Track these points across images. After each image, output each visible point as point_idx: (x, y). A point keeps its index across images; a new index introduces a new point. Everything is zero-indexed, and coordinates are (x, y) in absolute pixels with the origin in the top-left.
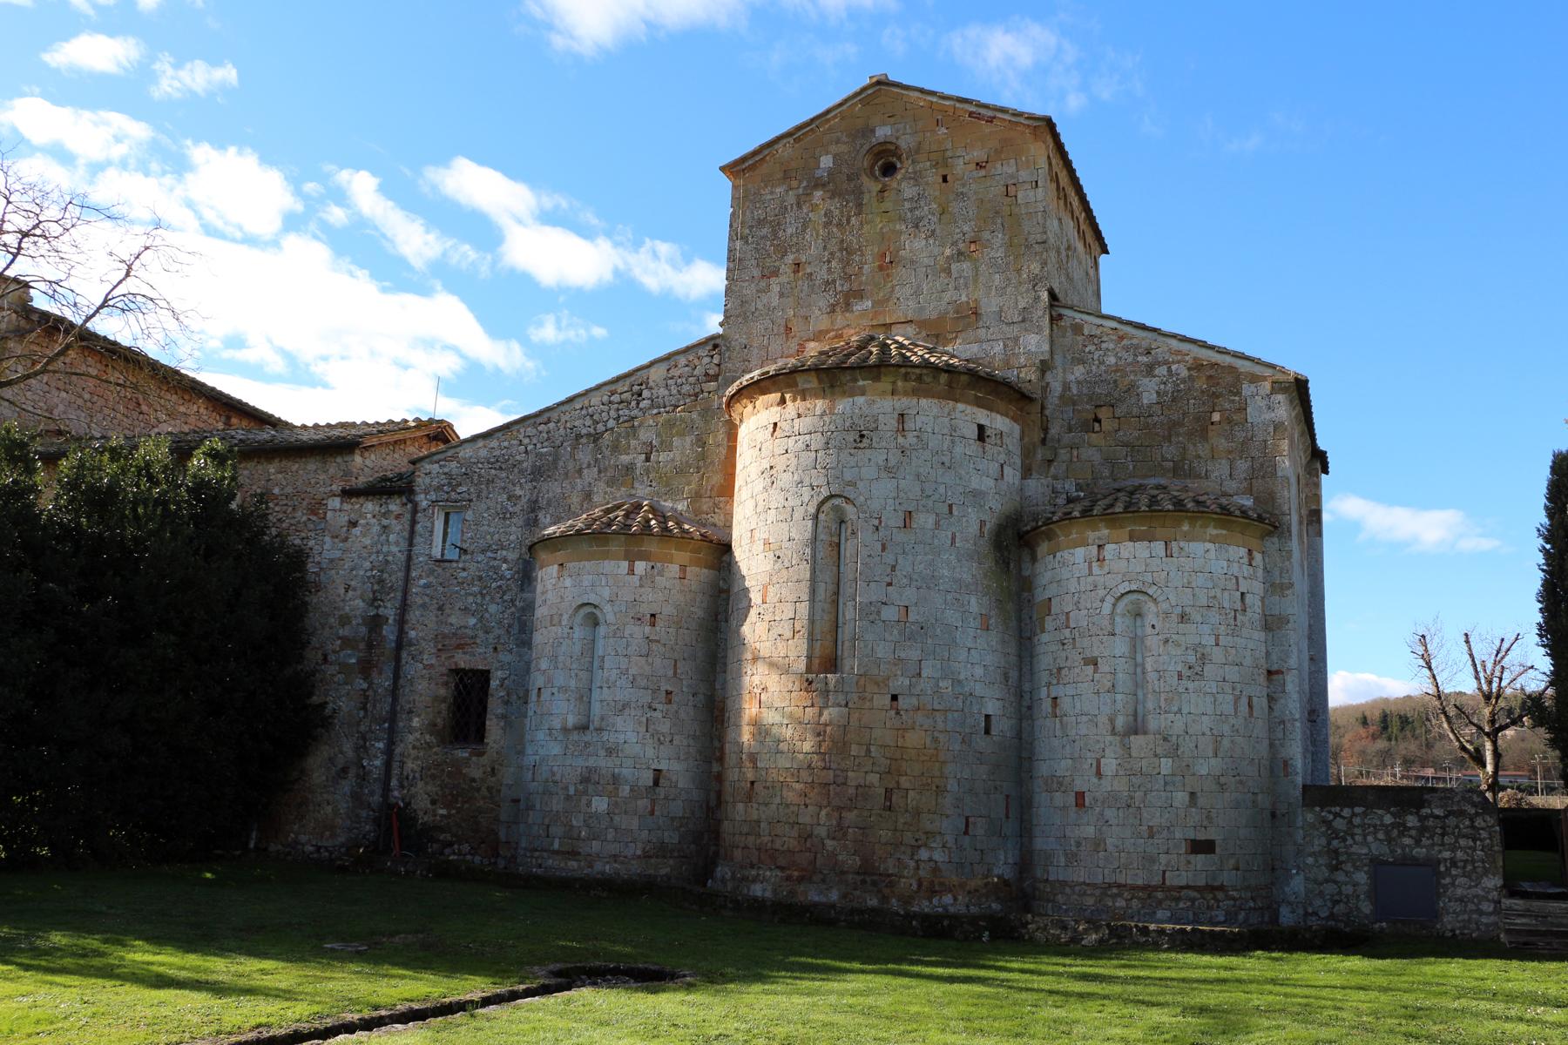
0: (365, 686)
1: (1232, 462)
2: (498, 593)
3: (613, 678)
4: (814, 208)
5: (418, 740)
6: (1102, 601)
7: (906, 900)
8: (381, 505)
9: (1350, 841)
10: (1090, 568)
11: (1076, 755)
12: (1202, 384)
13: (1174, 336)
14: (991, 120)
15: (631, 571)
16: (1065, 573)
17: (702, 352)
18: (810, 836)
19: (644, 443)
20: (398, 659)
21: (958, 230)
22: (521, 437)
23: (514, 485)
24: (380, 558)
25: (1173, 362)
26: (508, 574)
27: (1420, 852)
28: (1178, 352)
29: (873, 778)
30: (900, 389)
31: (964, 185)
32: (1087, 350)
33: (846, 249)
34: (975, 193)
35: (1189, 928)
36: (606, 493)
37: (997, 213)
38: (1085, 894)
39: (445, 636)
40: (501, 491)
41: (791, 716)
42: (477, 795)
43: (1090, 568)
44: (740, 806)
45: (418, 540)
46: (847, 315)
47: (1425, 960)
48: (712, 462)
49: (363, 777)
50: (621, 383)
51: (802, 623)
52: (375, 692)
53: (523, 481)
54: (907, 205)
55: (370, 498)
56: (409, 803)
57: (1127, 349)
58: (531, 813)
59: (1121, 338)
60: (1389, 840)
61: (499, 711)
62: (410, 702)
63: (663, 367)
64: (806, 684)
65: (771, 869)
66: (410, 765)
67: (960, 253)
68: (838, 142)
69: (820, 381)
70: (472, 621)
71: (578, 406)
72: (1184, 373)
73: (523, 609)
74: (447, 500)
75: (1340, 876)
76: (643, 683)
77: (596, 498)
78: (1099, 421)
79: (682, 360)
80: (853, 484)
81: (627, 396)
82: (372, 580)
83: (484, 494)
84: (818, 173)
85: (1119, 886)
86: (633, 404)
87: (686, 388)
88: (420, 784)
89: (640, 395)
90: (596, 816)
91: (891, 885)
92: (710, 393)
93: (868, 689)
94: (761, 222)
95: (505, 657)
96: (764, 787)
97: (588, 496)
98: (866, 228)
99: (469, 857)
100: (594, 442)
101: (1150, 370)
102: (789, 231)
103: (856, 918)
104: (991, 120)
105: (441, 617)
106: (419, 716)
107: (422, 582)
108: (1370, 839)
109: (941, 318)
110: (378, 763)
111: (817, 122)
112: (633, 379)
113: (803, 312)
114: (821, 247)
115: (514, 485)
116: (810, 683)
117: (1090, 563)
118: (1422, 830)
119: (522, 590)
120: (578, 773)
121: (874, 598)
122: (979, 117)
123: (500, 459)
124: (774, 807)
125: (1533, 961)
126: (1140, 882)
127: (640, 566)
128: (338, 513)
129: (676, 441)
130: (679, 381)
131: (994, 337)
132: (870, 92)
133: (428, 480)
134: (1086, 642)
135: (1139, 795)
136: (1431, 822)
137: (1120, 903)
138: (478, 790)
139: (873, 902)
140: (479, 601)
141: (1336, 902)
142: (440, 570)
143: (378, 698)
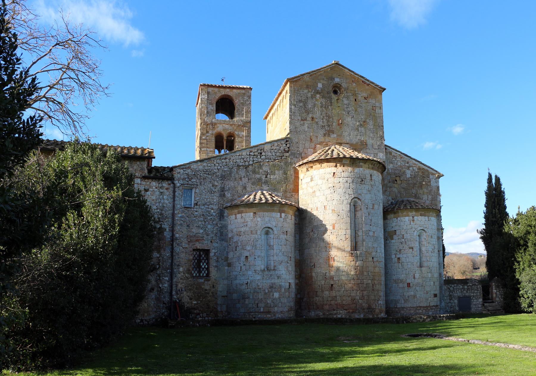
0: (158, 255)
1: (428, 196)
2: (211, 221)
3: (278, 253)
4: (317, 100)
5: (182, 276)
6: (414, 232)
7: (377, 315)
8: (159, 184)
9: (454, 293)
10: (410, 223)
11: (407, 273)
12: (420, 174)
13: (414, 159)
14: (368, 85)
15: (281, 217)
16: (402, 224)
17: (283, 142)
18: (355, 299)
19: (265, 171)
20: (172, 245)
21: (360, 117)
22: (215, 163)
23: (214, 181)
24: (161, 205)
25: (414, 167)
26: (214, 214)
27: (467, 294)
28: (415, 164)
29: (370, 281)
30: (370, 167)
31: (361, 104)
32: (393, 160)
33: (328, 116)
34: (364, 107)
35: (448, 315)
36: (251, 187)
37: (371, 114)
38: (411, 310)
39: (191, 237)
40: (209, 183)
41: (346, 264)
42: (208, 295)
43: (410, 223)
44: (327, 293)
45: (176, 199)
46: (329, 138)
47: (492, 317)
48: (290, 181)
49: (160, 291)
50: (254, 149)
51: (348, 236)
52: (163, 258)
53: (217, 180)
54: (345, 106)
55: (154, 180)
56: (181, 300)
57: (403, 161)
58: (247, 300)
59: (401, 158)
60: (462, 292)
61: (214, 264)
62: (178, 262)
63: (269, 145)
64: (351, 254)
65: (342, 310)
66: (180, 286)
67: (361, 125)
68: (323, 80)
69: (350, 162)
70: (201, 231)
71: (238, 155)
72: (417, 170)
73: (221, 227)
74: (187, 184)
75: (452, 301)
76: (285, 254)
77: (248, 189)
78: (396, 181)
79: (276, 144)
80: (360, 194)
81: (256, 153)
82: (157, 213)
83: (203, 183)
84: (318, 89)
85: (420, 307)
86: (259, 156)
87: (278, 154)
88: (185, 293)
89: (261, 154)
90: (275, 299)
91: (374, 311)
92: (286, 157)
93: (367, 256)
94: (300, 101)
95: (215, 245)
96: (338, 286)
97: (245, 188)
98: (334, 111)
99: (206, 318)
100: (245, 168)
101: (408, 168)
102: (309, 106)
103: (383, 320)
104: (368, 85)
105: (188, 229)
106: (182, 267)
107: (180, 215)
108: (458, 292)
109: (357, 143)
110: (166, 285)
111: (317, 71)
112: (258, 148)
113: (315, 134)
114: (320, 114)
115: (214, 181)
116: (352, 254)
117: (410, 221)
118: (468, 289)
119: (220, 220)
120: (269, 285)
121: (368, 229)
122: (365, 83)
123: (208, 170)
124: (342, 292)
125: (475, 318)
126: (425, 305)
127: (283, 215)
128: (139, 185)
129: (277, 172)
130: (275, 151)
131: (371, 152)
132: (333, 65)
133: (179, 176)
134: (410, 243)
135: (424, 283)
136: (469, 287)
137: (421, 311)
138: (208, 293)
139: (371, 317)
140: (204, 224)
141: (451, 308)
142: (186, 211)
143: (164, 260)
